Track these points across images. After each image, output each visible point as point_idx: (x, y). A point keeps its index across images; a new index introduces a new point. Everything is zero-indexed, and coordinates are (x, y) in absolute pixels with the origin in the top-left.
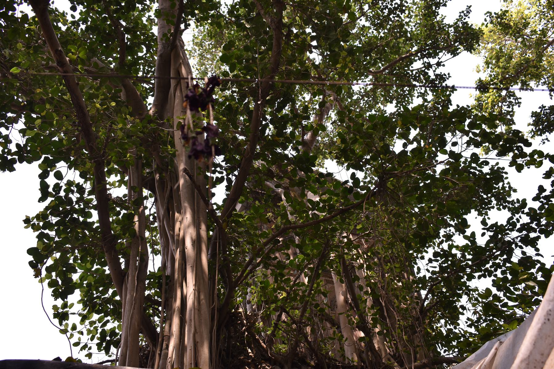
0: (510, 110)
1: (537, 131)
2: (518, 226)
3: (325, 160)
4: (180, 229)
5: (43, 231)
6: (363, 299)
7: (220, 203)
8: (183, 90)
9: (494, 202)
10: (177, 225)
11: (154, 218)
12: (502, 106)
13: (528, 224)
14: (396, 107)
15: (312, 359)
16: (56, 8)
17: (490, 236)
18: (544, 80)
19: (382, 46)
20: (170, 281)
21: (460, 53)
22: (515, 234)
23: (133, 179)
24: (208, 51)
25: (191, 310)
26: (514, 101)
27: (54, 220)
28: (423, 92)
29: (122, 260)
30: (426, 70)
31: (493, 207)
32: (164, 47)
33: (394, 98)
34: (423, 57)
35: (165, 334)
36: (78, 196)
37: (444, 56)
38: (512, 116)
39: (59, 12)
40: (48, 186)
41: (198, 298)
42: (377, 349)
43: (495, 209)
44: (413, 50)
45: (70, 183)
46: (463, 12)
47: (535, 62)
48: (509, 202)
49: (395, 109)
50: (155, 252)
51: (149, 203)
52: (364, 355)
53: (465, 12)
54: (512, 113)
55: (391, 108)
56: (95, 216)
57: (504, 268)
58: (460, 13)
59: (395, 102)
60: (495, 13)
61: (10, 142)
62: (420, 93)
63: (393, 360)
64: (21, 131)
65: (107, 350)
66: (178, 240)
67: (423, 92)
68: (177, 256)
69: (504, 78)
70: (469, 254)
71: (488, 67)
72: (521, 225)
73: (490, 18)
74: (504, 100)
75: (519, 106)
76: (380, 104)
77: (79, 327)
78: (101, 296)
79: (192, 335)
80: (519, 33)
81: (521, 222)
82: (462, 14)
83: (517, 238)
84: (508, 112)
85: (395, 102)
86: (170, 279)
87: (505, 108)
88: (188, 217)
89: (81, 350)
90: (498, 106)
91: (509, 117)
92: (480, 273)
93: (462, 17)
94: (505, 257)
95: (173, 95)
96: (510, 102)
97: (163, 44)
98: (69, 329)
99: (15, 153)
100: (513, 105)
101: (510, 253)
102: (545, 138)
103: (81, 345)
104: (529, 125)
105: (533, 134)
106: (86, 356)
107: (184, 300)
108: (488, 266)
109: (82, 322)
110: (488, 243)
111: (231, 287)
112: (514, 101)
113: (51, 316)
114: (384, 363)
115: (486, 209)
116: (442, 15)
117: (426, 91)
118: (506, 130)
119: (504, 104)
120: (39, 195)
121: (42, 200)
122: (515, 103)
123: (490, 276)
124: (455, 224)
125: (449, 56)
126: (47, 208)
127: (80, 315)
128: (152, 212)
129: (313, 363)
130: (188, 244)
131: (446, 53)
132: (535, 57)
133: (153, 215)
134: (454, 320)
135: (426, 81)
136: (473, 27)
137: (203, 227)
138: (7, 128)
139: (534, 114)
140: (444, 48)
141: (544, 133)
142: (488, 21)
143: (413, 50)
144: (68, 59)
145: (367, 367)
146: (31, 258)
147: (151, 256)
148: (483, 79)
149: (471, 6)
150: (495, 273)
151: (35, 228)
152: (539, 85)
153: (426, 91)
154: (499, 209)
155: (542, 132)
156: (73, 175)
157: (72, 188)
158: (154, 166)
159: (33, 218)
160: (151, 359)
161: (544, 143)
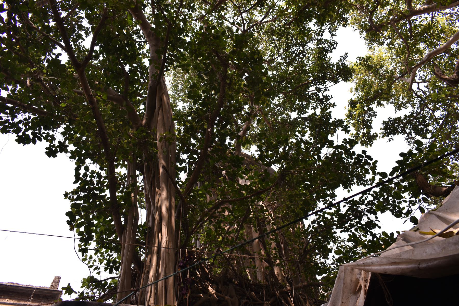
0: (370, 119)
1: (386, 133)
2: (366, 202)
3: (251, 146)
4: (158, 199)
5: (76, 202)
6: (269, 243)
7: (184, 181)
8: (164, 111)
9: (355, 180)
10: (157, 197)
11: (142, 188)
12: (364, 116)
13: (371, 201)
14: (297, 114)
15: (236, 279)
16: (84, 46)
17: (349, 206)
18: (392, 101)
19: (290, 79)
20: (151, 231)
21: (340, 82)
22: (363, 207)
23: (131, 168)
24: (179, 73)
25: (164, 253)
26: (372, 114)
27: (82, 194)
28: (315, 106)
29: (122, 219)
30: (318, 93)
31: (354, 183)
32: (153, 82)
33: (297, 109)
34: (316, 84)
35: (147, 264)
36: (98, 179)
37: (329, 84)
38: (371, 123)
39: (85, 49)
40: (80, 174)
41: (169, 242)
42: (276, 274)
43: (356, 184)
44: (310, 80)
45: (93, 172)
46: (342, 56)
47: (386, 91)
48: (364, 181)
49: (297, 116)
50: (141, 207)
51: (140, 179)
52: (268, 277)
53: (344, 57)
54: (371, 121)
55: (294, 115)
56: (107, 193)
57: (356, 227)
58: (341, 57)
59: (297, 111)
60: (363, 58)
61: (55, 139)
62: (313, 107)
63: (286, 281)
64: (62, 133)
65: (111, 272)
66: (157, 207)
67: (315, 106)
68: (157, 216)
69: (367, 99)
70: (336, 217)
71: (357, 92)
72: (367, 202)
73: (360, 61)
74: (366, 113)
75: (375, 117)
76: (287, 111)
77: (94, 257)
78: (108, 238)
79: (164, 269)
80: (377, 72)
81: (368, 200)
82: (342, 58)
83: (365, 209)
84: (368, 121)
85: (297, 111)
86: (151, 229)
87: (366, 118)
88: (164, 194)
89: (94, 270)
90: (362, 116)
91: (368, 123)
92: (342, 230)
93: (342, 60)
94: (357, 220)
95: (157, 113)
96: (370, 114)
97: (152, 80)
98: (88, 258)
99: (58, 147)
100: (371, 116)
101: (361, 219)
102: (391, 138)
103: (94, 267)
104: (381, 129)
105: (383, 135)
106: (97, 273)
107: (160, 244)
108: (347, 225)
109: (96, 254)
110: (348, 210)
111: (188, 234)
112: (372, 114)
113: (77, 251)
114: (280, 283)
115: (350, 184)
116: (330, 57)
117: (317, 106)
118: (366, 131)
119: (366, 115)
120: (74, 179)
121: (76, 182)
122: (373, 115)
123: (348, 232)
124: (330, 193)
125: (332, 83)
126: (78, 188)
127: (94, 249)
128: (141, 185)
129: (236, 282)
130: (164, 210)
131: (331, 82)
132: (386, 88)
133: (142, 186)
134: (326, 257)
135: (317, 100)
136: (348, 66)
137: (173, 200)
138: (53, 131)
139: (384, 123)
140: (329, 79)
141: (390, 135)
142: (358, 63)
143: (310, 80)
144: (95, 99)
145: (269, 286)
146: (68, 218)
147: (139, 209)
148: (353, 99)
149: (348, 53)
150: (351, 230)
151: (71, 199)
152: (389, 103)
153: (317, 106)
154: (358, 185)
155: (389, 134)
156: (95, 167)
157: (94, 175)
158: (144, 158)
159: (70, 193)
160: (138, 278)
161: (390, 141)
